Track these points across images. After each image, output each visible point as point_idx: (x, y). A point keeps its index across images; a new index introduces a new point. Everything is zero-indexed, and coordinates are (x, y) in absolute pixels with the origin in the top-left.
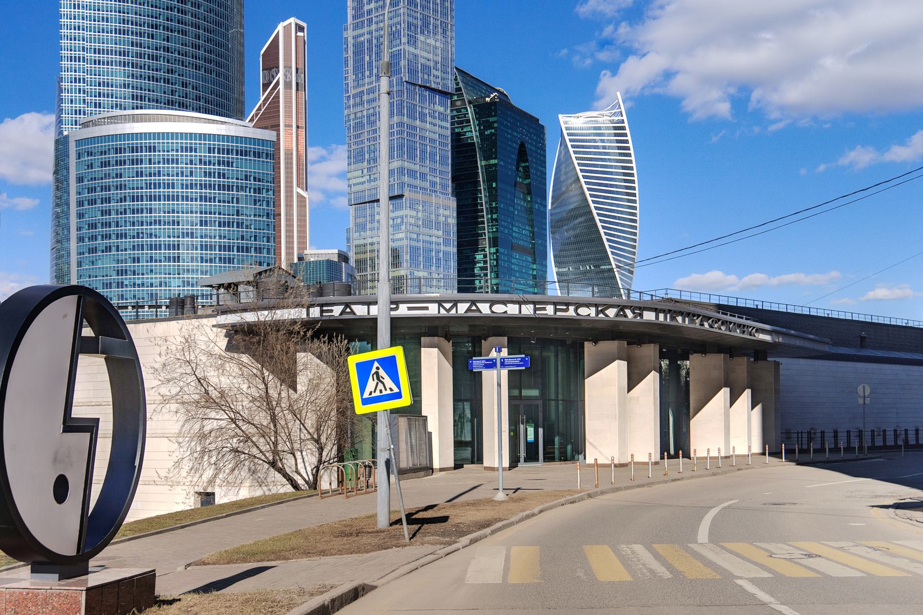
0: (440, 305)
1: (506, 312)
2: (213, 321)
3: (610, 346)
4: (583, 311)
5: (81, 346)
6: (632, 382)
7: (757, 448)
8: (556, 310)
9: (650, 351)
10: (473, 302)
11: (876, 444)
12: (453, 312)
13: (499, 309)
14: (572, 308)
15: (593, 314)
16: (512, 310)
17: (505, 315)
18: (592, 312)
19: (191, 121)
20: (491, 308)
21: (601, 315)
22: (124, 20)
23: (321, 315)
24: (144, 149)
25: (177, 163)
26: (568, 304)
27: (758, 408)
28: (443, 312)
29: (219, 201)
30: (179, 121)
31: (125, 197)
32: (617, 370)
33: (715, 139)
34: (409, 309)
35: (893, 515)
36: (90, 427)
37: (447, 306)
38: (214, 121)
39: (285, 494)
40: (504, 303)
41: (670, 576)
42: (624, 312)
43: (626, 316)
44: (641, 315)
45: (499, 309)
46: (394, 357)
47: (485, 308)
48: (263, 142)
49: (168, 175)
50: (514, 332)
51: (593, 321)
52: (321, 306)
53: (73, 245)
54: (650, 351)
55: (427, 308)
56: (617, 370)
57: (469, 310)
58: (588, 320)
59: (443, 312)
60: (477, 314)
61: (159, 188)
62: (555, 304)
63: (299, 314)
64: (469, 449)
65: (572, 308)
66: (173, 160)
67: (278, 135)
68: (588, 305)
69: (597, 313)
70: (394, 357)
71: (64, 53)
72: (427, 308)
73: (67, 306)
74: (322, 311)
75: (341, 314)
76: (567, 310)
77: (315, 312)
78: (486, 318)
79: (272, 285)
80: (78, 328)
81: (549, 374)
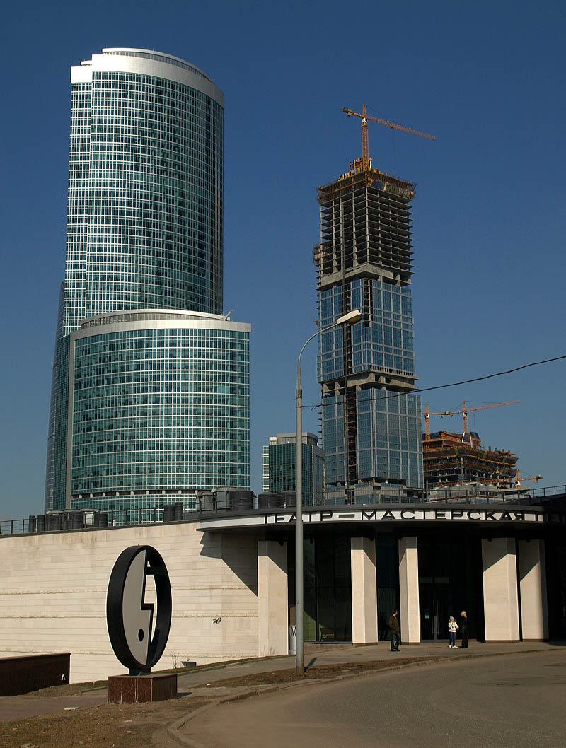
0: (363, 513)
1: (414, 518)
2: (199, 525)
3: (502, 542)
4: (475, 516)
5: (148, 571)
6: (521, 574)
7: (534, 630)
8: (453, 515)
9: (536, 546)
10: (389, 511)
11: (25, 532)
12: (373, 518)
13: (408, 515)
14: (465, 514)
15: (483, 518)
16: (419, 516)
17: (413, 520)
18: (482, 516)
19: (188, 318)
20: (402, 514)
21: (489, 518)
22: (129, 278)
23: (321, 520)
24: (134, 344)
25: (179, 391)
26: (462, 511)
27: (183, 666)
28: (365, 518)
29: (183, 346)
30: (176, 318)
31: (115, 446)
32: (507, 563)
33: (467, 484)
34: (340, 516)
35: (136, 532)
36: (150, 607)
37: (369, 514)
38: (199, 317)
39: (181, 668)
40: (412, 510)
41: (510, 514)
42: (509, 516)
43: (510, 519)
44: (523, 517)
45: (408, 515)
46: (142, 609)
47: (397, 515)
48: (240, 334)
49: (171, 356)
50: (424, 535)
51: (485, 523)
52: (276, 515)
53: (70, 456)
54: (536, 546)
55: (353, 516)
56: (507, 563)
57: (385, 516)
58: (476, 523)
59: (365, 518)
60: (391, 520)
61: (83, 90)
62: (452, 511)
63: (259, 521)
64: (388, 625)
65: (465, 514)
66: (175, 387)
67: (302, 441)
68: (478, 511)
69: (486, 516)
70: (142, 609)
71: (71, 216)
72: (353, 516)
73: (143, 553)
74: (276, 519)
75: (290, 521)
76: (461, 515)
77: (271, 520)
78: (398, 522)
79: (242, 501)
80: (146, 564)
81: (556, 645)
